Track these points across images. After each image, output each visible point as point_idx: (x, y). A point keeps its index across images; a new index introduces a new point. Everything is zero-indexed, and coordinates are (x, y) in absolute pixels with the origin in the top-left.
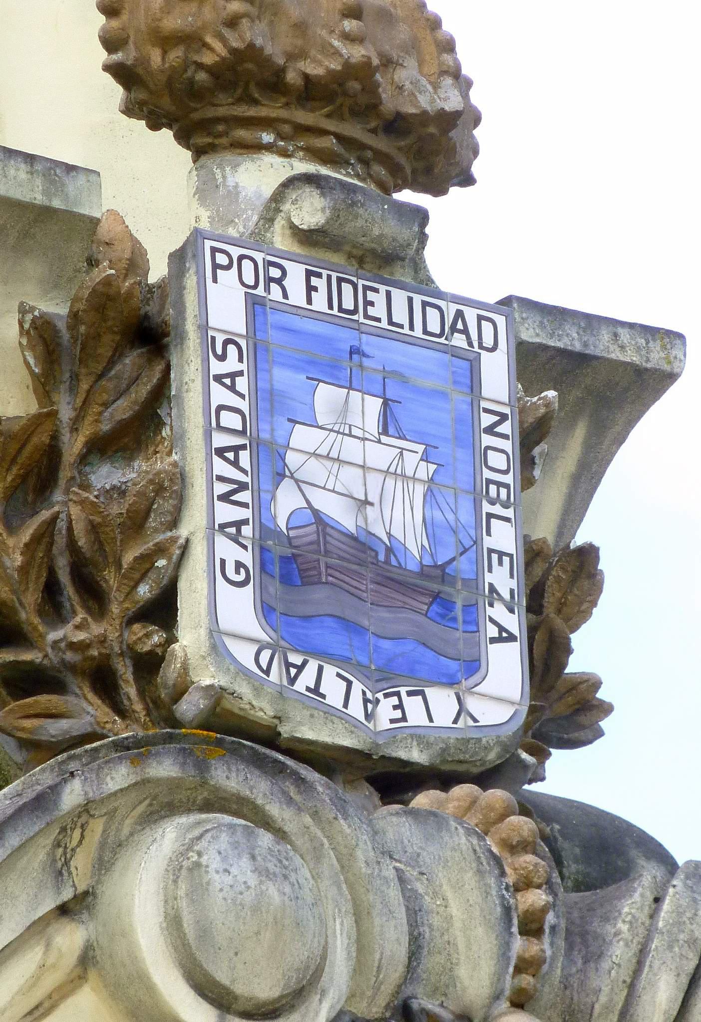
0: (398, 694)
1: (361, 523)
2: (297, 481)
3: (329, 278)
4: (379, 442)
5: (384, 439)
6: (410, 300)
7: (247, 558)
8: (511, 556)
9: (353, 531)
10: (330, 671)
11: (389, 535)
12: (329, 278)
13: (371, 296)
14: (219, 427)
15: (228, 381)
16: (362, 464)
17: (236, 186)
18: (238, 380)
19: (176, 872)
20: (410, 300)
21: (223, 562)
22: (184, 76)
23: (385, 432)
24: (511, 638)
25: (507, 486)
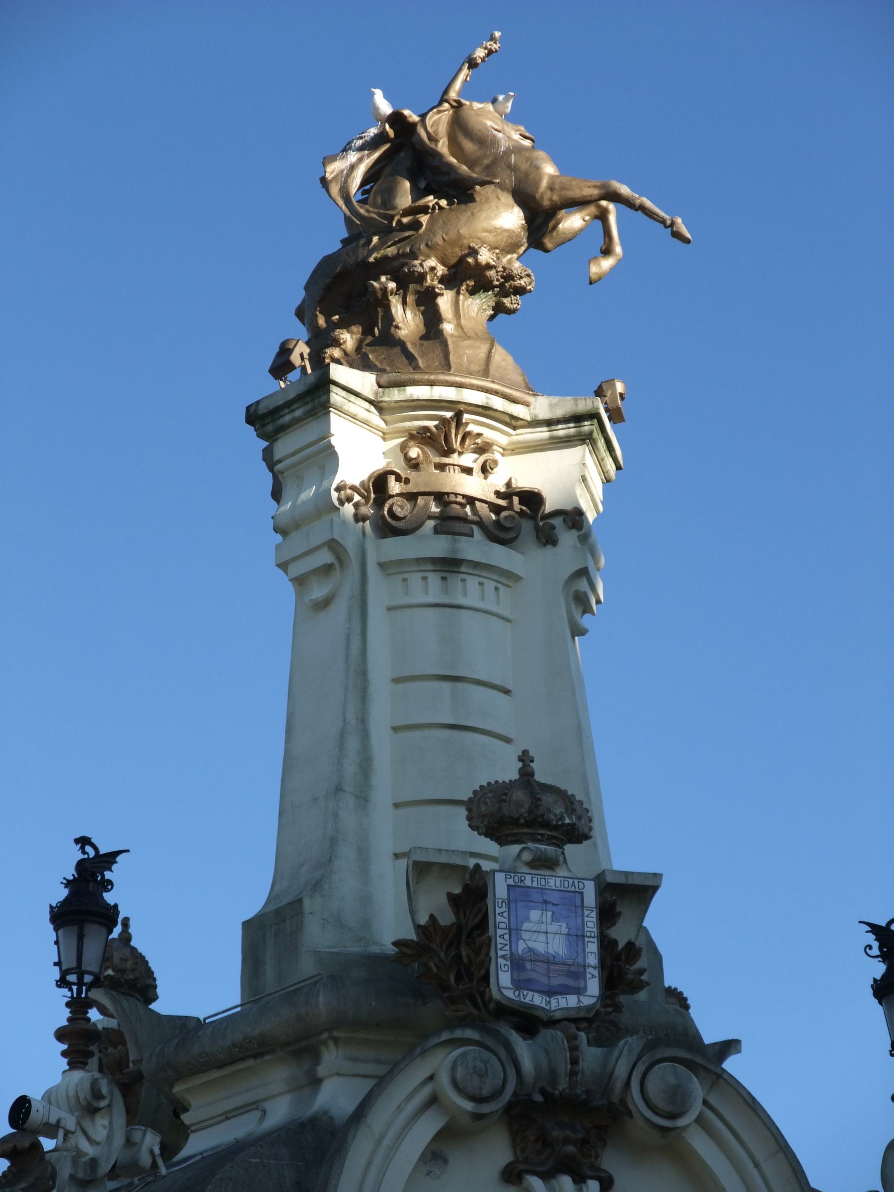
0: (558, 999)
1: (546, 950)
2: (524, 940)
3: (538, 878)
4: (551, 924)
5: (552, 923)
6: (561, 880)
7: (509, 963)
8: (595, 953)
9: (543, 953)
10: (536, 995)
11: (554, 952)
12: (538, 878)
13: (549, 880)
14: (499, 928)
15: (502, 937)
16: (545, 931)
17: (395, 944)
18: (505, 936)
19: (523, 270)
20: (561, 880)
21: (501, 964)
22: (320, 490)
23: (553, 921)
24: (595, 977)
25: (594, 932)
